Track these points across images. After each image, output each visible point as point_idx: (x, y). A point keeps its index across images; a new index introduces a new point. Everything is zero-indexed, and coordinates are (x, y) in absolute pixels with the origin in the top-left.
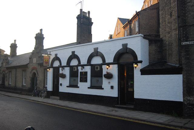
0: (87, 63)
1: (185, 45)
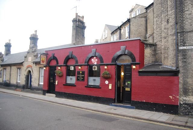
1: (183, 50)
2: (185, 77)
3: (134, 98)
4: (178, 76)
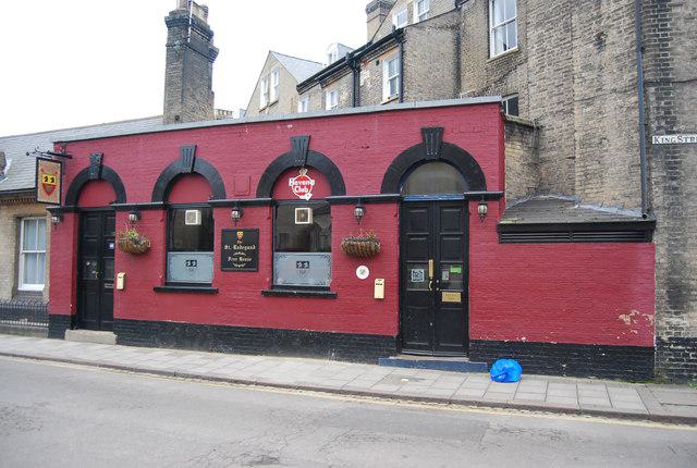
1: (665, 146)
2: (677, 243)
3: (477, 330)
4: (650, 240)
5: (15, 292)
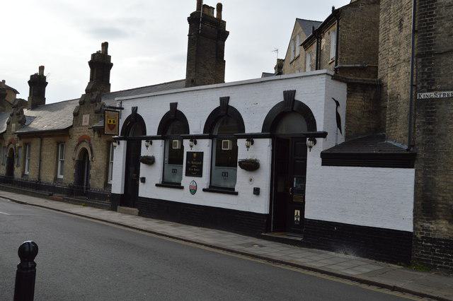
0: (205, 131)
5: (56, 179)
